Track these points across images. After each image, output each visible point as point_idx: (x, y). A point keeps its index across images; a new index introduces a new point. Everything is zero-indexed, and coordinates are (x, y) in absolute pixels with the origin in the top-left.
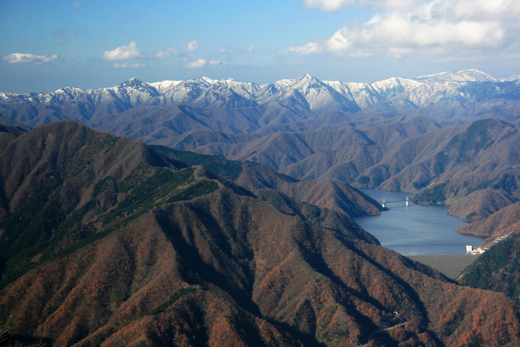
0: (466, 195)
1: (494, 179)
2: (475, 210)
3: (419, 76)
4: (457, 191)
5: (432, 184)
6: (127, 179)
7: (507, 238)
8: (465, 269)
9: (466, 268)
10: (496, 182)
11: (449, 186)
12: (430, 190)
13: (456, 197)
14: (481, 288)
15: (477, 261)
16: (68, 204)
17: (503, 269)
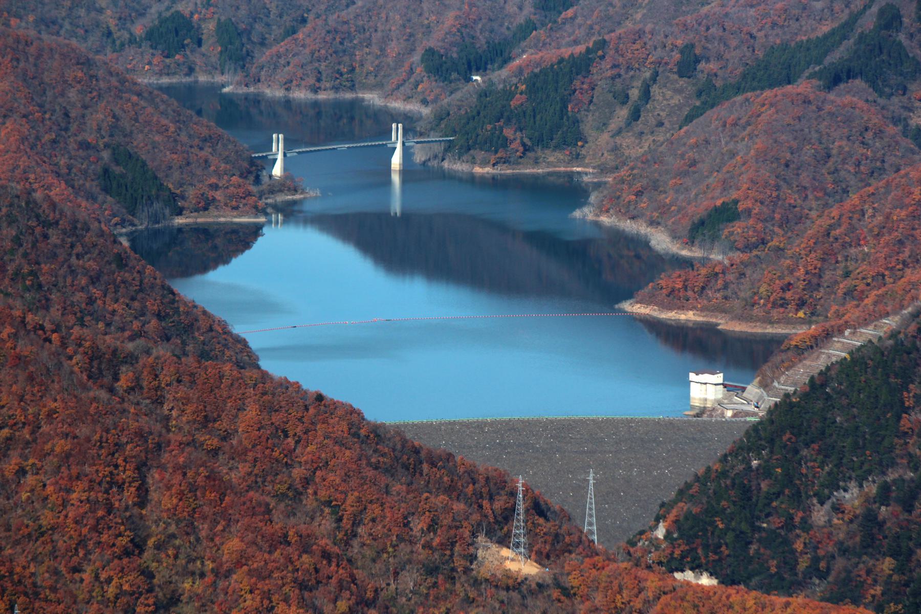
0: (689, 119)
1: (833, 33)
2: (734, 194)
3: (257, 153)
4: (646, 95)
5: (524, 58)
6: (137, 481)
7: (894, 335)
8: (681, 492)
9: (688, 486)
10: (837, 56)
11: (602, 71)
12: (509, 94)
13: (639, 126)
14: (759, 587)
15: (740, 450)
16: (325, 524)
17: (871, 488)
